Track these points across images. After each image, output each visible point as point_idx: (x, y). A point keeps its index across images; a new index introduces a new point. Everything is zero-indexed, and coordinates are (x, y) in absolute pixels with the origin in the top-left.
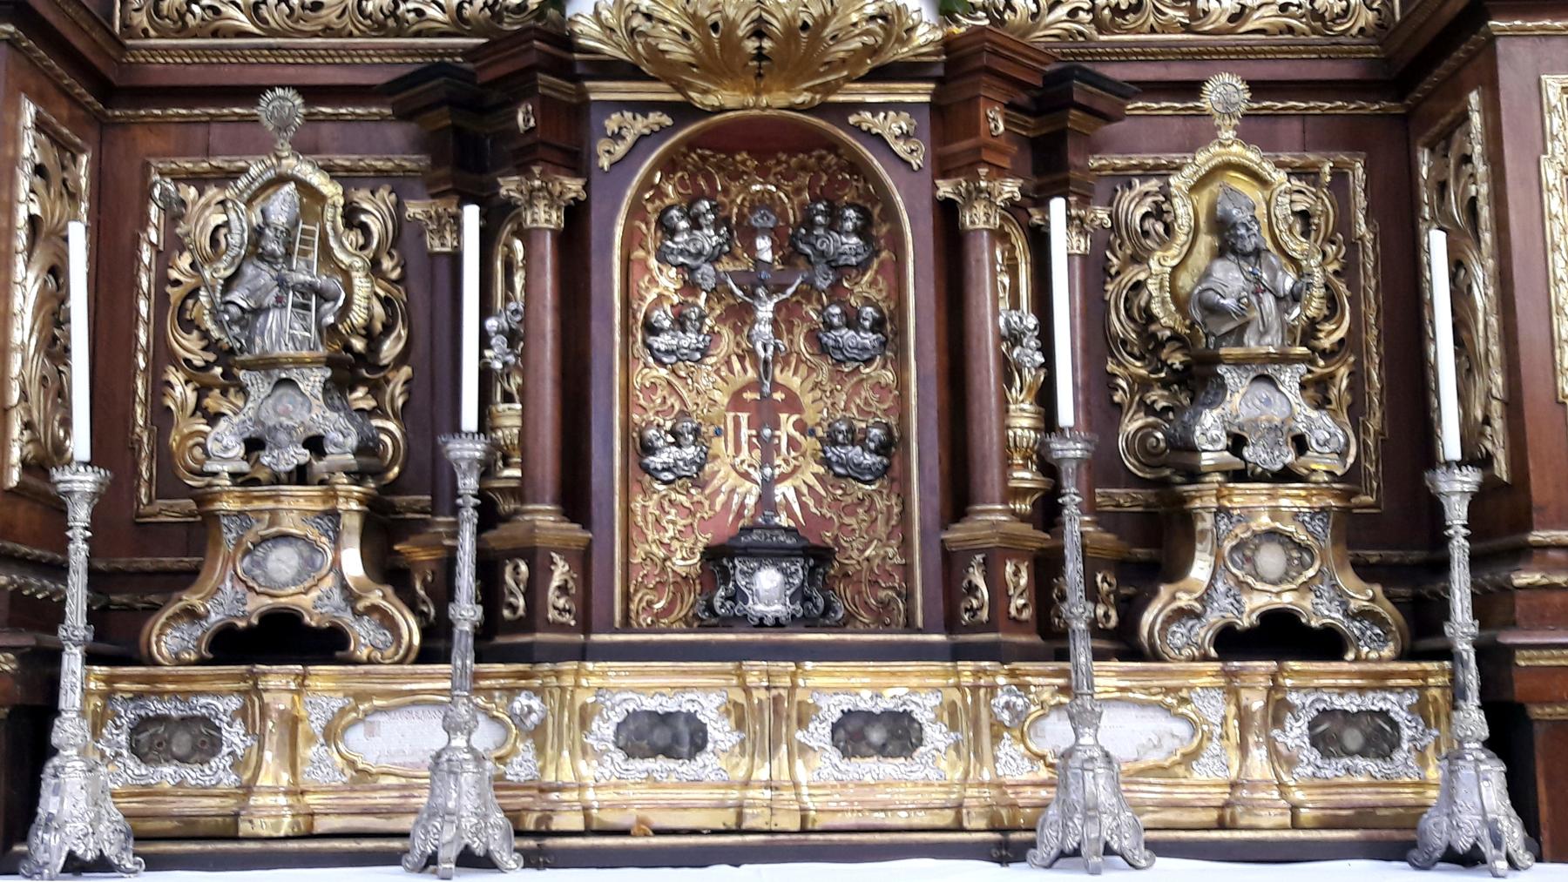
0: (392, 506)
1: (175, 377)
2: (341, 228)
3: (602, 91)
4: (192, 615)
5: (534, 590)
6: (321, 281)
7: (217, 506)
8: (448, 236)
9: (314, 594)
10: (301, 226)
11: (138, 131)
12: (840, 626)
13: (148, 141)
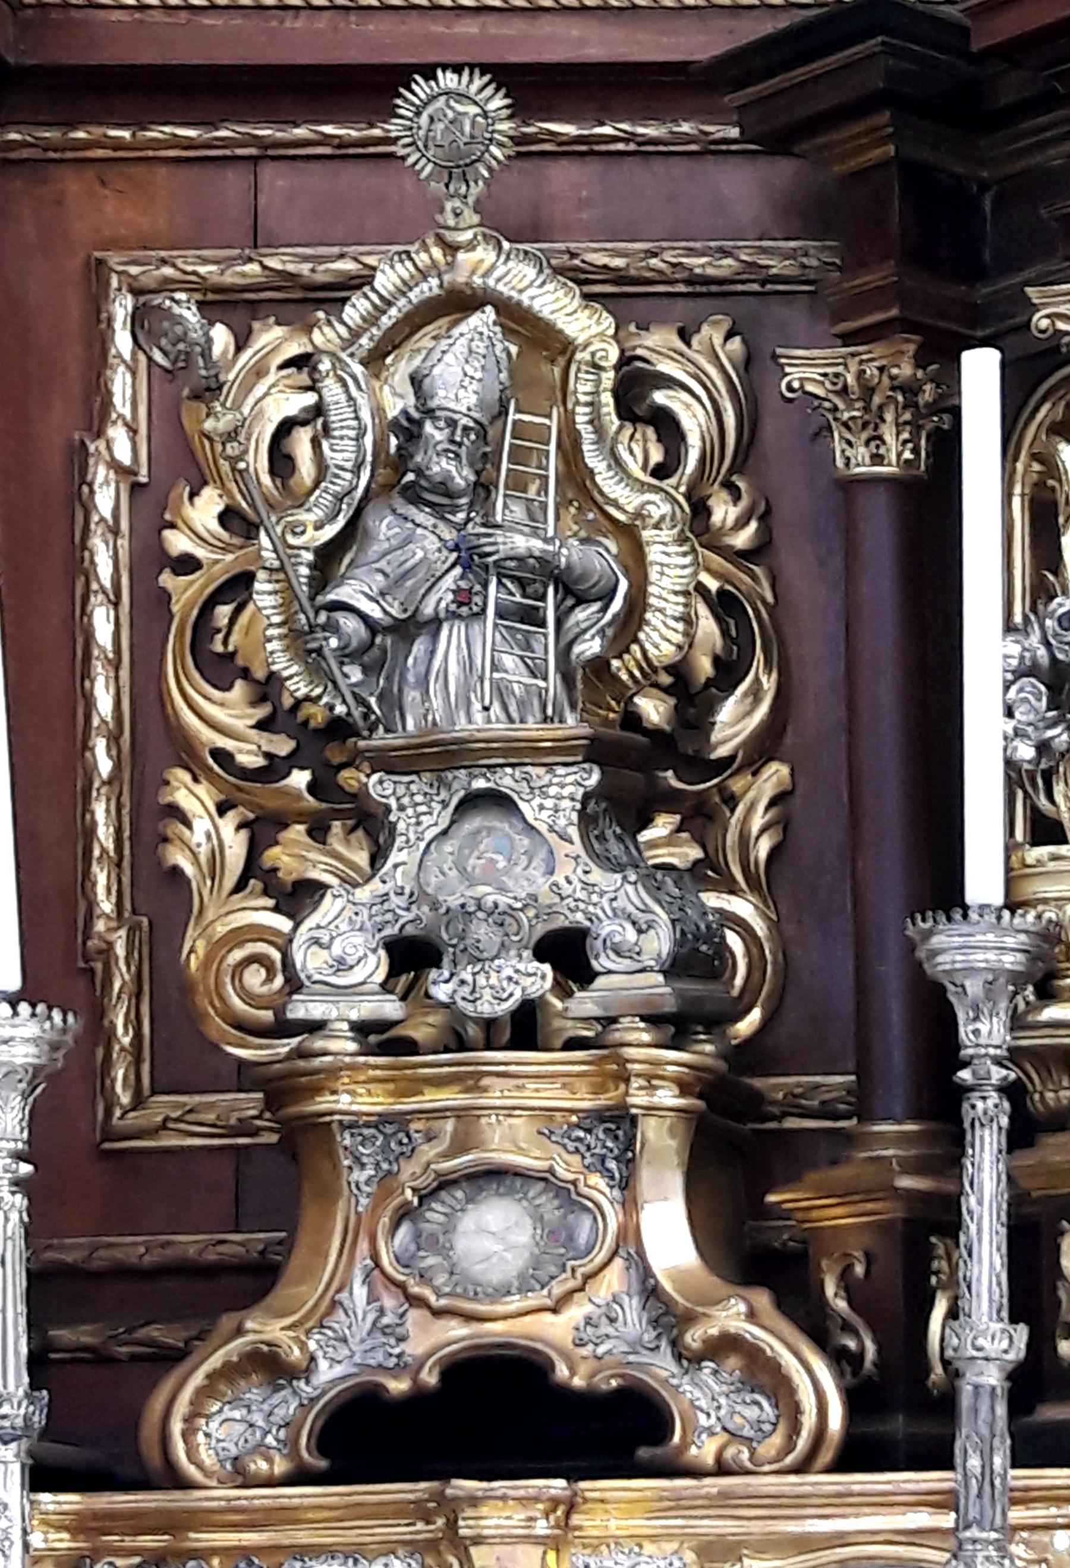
0: (758, 1098)
1: (192, 796)
2: (613, 421)
4: (272, 1367)
6: (571, 553)
7: (323, 1103)
8: (889, 437)
9: (576, 1312)
10: (512, 416)
11: (73, 184)
13: (96, 209)
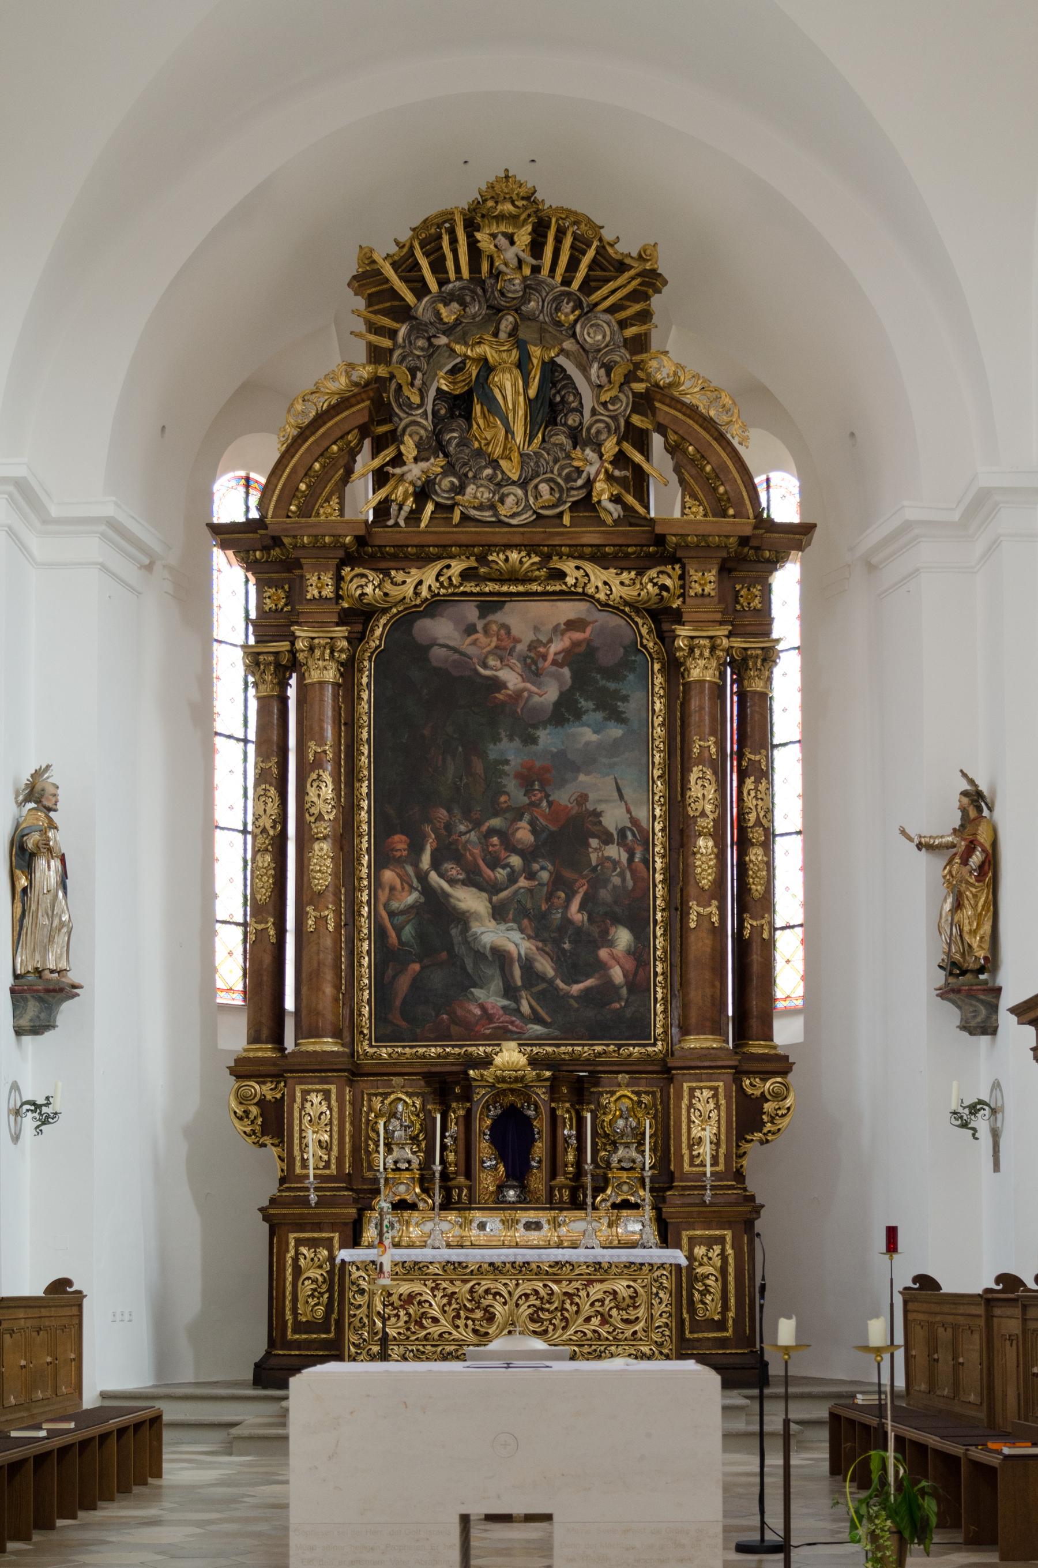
3: (474, 1084)
5: (459, 1195)
12: (528, 1203)
